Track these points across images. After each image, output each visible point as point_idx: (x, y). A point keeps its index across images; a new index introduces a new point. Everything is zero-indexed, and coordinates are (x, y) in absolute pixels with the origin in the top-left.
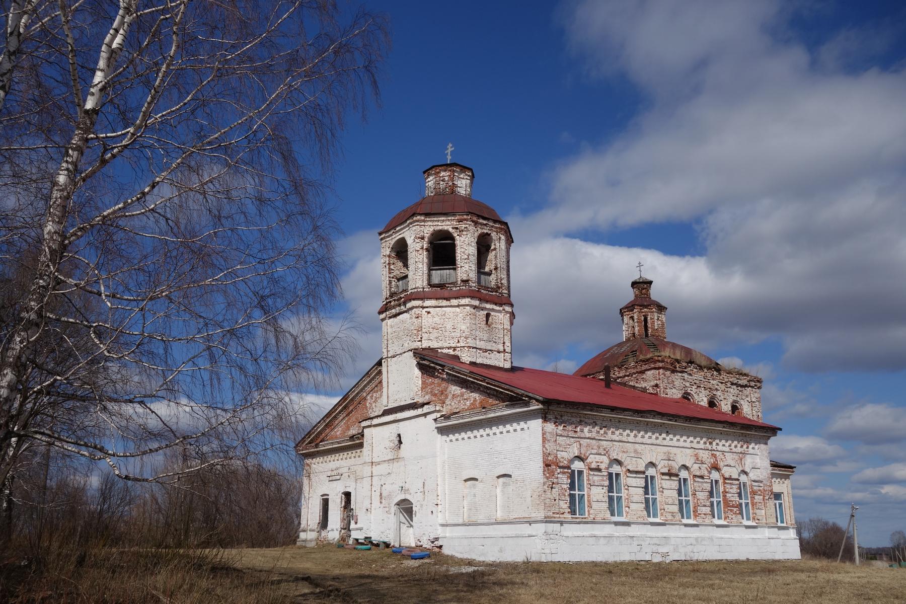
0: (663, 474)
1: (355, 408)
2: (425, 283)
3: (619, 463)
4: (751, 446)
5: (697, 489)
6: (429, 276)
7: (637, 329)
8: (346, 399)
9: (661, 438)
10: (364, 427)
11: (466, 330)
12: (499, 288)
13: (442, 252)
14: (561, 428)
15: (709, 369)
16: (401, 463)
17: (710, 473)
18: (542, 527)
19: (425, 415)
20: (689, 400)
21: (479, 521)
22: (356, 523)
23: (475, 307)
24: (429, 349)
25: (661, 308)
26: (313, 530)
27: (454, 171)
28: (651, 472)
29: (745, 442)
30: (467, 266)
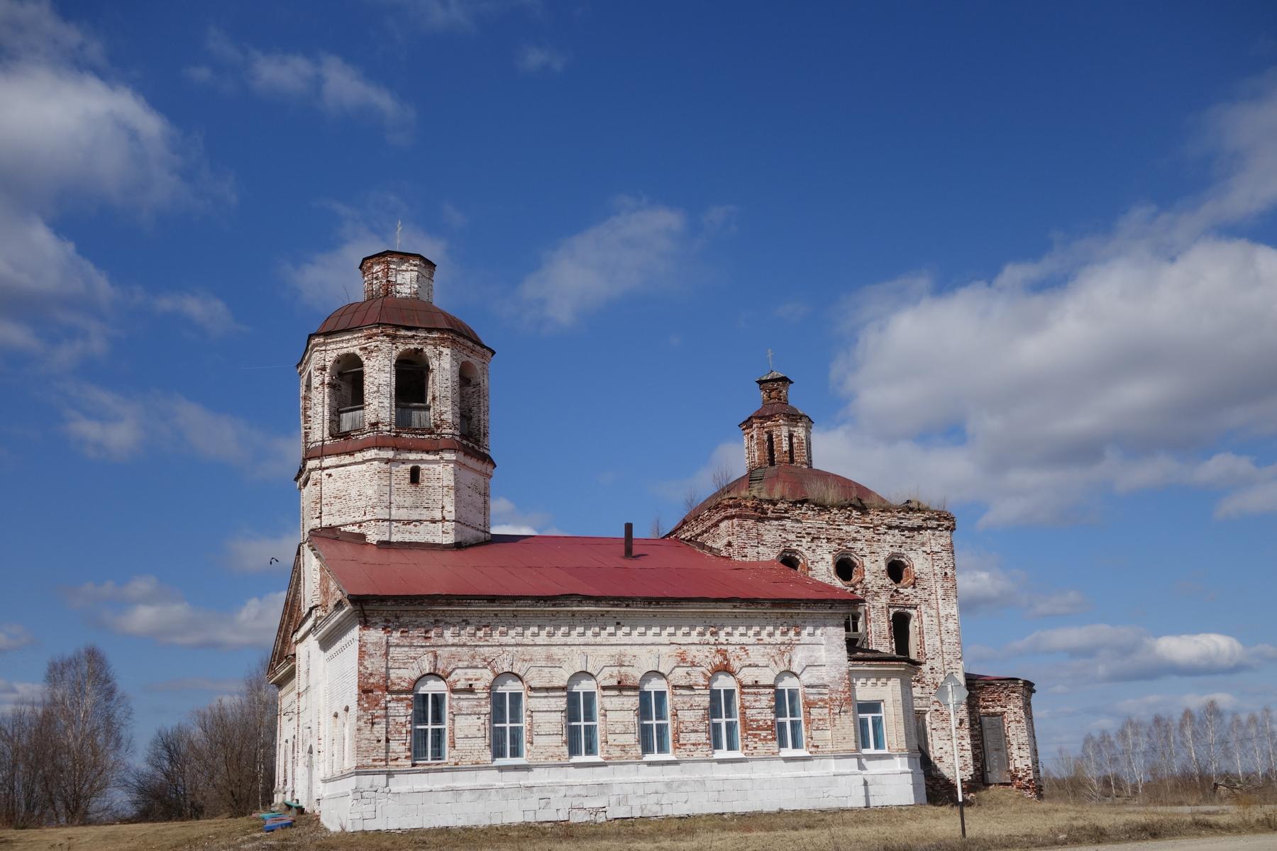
0: (604, 688)
2: (327, 432)
4: (805, 633)
12: (437, 427)
14: (396, 634)
15: (841, 507)
18: (352, 782)
27: (388, 263)
28: (584, 686)
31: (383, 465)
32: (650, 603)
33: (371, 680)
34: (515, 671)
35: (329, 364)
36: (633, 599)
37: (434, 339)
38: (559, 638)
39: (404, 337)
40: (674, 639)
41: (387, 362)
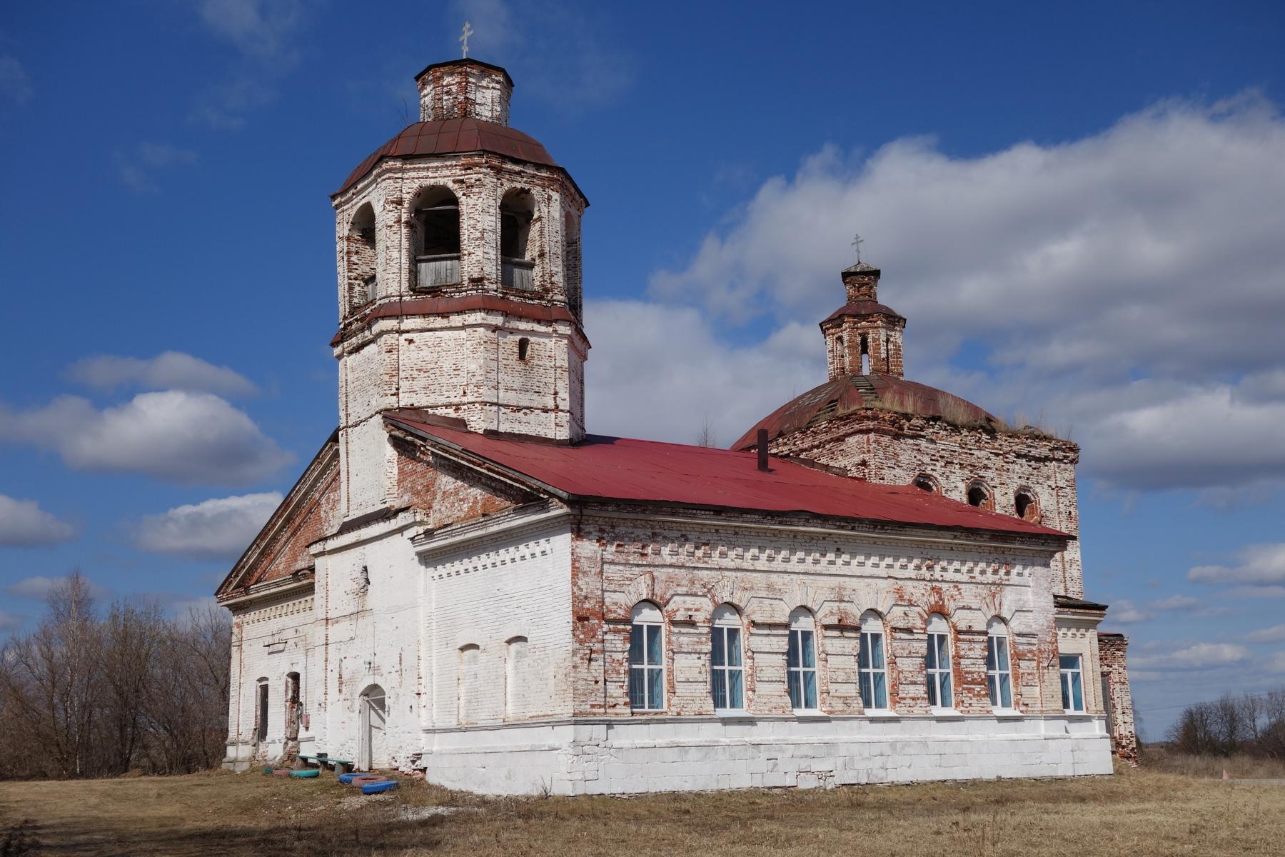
0: (827, 627)
1: (304, 521)
2: (405, 285)
3: (737, 610)
4: (1014, 572)
5: (898, 652)
6: (414, 274)
7: (847, 359)
8: (288, 506)
9: (824, 561)
10: (316, 555)
11: (478, 372)
12: (547, 291)
13: (436, 227)
14: (612, 548)
15: (972, 429)
16: (369, 619)
17: (927, 622)
18: (568, 732)
19: (401, 530)
20: (929, 488)
21: (481, 723)
22: (307, 728)
23: (495, 329)
24: (413, 409)
25: (894, 320)
26: (246, 743)
27: (467, 75)
28: (804, 624)
29: (1001, 564)
30: (479, 252)
31: (489, 333)
32: (875, 527)
33: (587, 605)
34: (736, 602)
35: (407, 197)
36: (854, 520)
37: (542, 178)
38: (778, 564)
39: (510, 172)
40: (892, 572)
41: (492, 202)
